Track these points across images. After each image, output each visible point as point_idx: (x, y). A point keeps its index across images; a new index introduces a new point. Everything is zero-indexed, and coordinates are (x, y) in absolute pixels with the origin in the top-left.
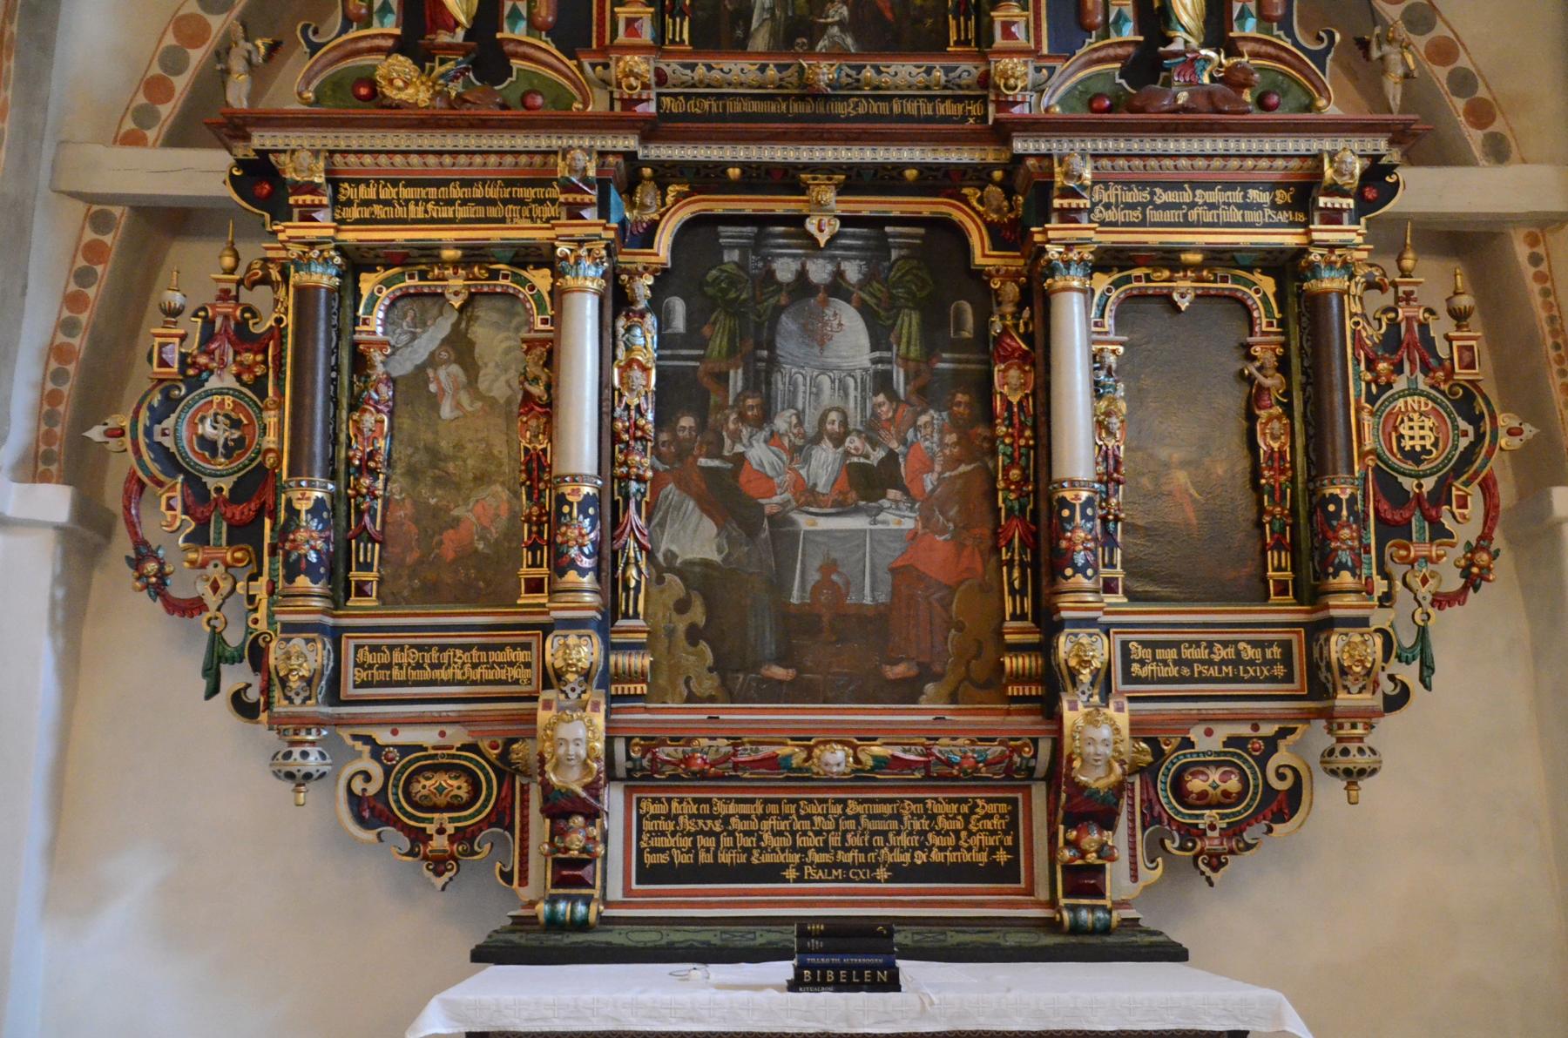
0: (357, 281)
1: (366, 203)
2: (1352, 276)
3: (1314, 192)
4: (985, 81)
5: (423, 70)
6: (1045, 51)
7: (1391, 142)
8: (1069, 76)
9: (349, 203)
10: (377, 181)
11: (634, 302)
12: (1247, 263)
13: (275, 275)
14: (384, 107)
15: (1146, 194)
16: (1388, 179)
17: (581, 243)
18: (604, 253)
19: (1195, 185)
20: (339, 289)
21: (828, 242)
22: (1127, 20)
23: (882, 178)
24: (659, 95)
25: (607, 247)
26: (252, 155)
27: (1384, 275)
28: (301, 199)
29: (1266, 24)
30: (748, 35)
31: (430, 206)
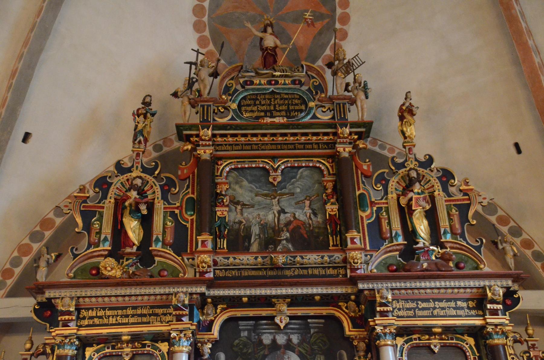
0: (84, 351)
1: (92, 318)
2: (507, 338)
3: (485, 303)
4: (345, 260)
5: (119, 262)
6: (368, 248)
7: (513, 282)
8: (379, 257)
9: (84, 318)
10: (97, 308)
11: (203, 355)
12: (460, 332)
13: (48, 350)
14: (102, 279)
15: (415, 304)
16: (515, 296)
17: (181, 331)
18: (191, 335)
19: (435, 300)
20: (76, 355)
21: (285, 327)
22: (399, 236)
23: (306, 300)
24: (214, 269)
25: (192, 333)
26: (44, 300)
27: (521, 336)
28: (63, 318)
29: (454, 236)
30: (250, 245)
31: (118, 318)
